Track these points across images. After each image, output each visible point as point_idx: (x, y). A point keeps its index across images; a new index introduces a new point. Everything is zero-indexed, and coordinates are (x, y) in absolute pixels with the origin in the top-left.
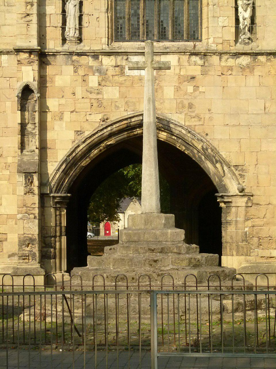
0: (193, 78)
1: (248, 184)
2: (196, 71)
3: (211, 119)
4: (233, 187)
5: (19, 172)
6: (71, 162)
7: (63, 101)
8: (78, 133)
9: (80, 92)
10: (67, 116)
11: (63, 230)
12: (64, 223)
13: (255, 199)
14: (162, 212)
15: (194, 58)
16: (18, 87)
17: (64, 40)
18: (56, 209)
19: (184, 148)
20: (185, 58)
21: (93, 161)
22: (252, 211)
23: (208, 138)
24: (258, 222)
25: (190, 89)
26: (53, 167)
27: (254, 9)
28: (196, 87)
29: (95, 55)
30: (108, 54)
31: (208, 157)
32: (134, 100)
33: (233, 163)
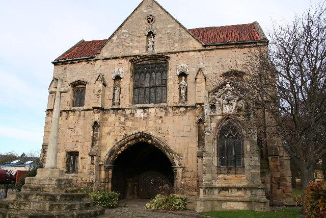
0: (161, 117)
1: (184, 163)
2: (163, 114)
3: (168, 134)
4: (177, 163)
5: (89, 155)
6: (112, 152)
7: (111, 128)
8: (116, 140)
9: (117, 124)
10: (111, 133)
11: (110, 180)
12: (110, 177)
13: (186, 169)
14: (254, 23)
15: (162, 109)
16: (92, 122)
17: (113, 104)
18: (105, 171)
19: (123, 148)
20: (158, 109)
21: (122, 153)
22: (186, 174)
23: (167, 142)
24: (187, 179)
25: (160, 121)
26: (104, 155)
27: (187, 89)
28: (162, 121)
29: (124, 110)
30: (129, 109)
31: (167, 150)
32: (200, 164)
33: (177, 153)
